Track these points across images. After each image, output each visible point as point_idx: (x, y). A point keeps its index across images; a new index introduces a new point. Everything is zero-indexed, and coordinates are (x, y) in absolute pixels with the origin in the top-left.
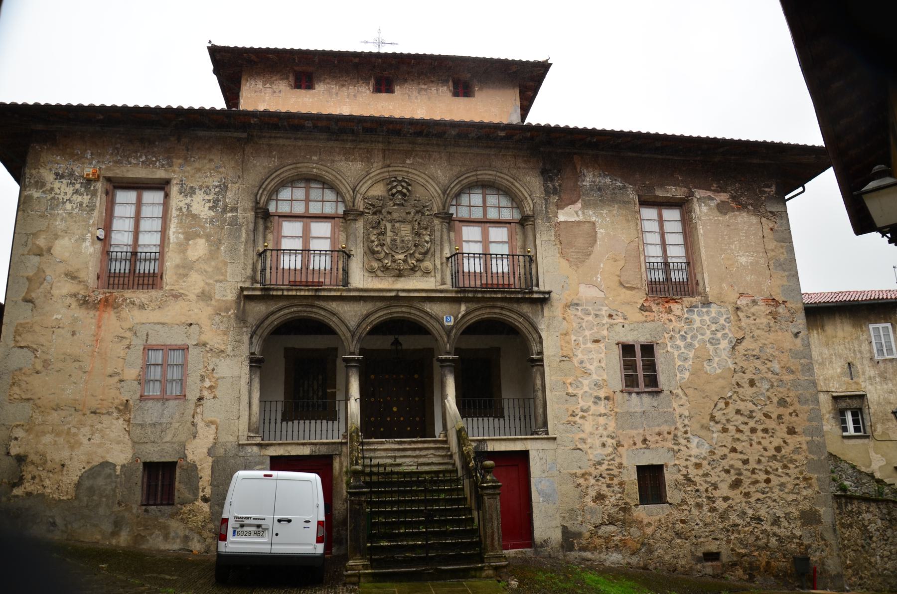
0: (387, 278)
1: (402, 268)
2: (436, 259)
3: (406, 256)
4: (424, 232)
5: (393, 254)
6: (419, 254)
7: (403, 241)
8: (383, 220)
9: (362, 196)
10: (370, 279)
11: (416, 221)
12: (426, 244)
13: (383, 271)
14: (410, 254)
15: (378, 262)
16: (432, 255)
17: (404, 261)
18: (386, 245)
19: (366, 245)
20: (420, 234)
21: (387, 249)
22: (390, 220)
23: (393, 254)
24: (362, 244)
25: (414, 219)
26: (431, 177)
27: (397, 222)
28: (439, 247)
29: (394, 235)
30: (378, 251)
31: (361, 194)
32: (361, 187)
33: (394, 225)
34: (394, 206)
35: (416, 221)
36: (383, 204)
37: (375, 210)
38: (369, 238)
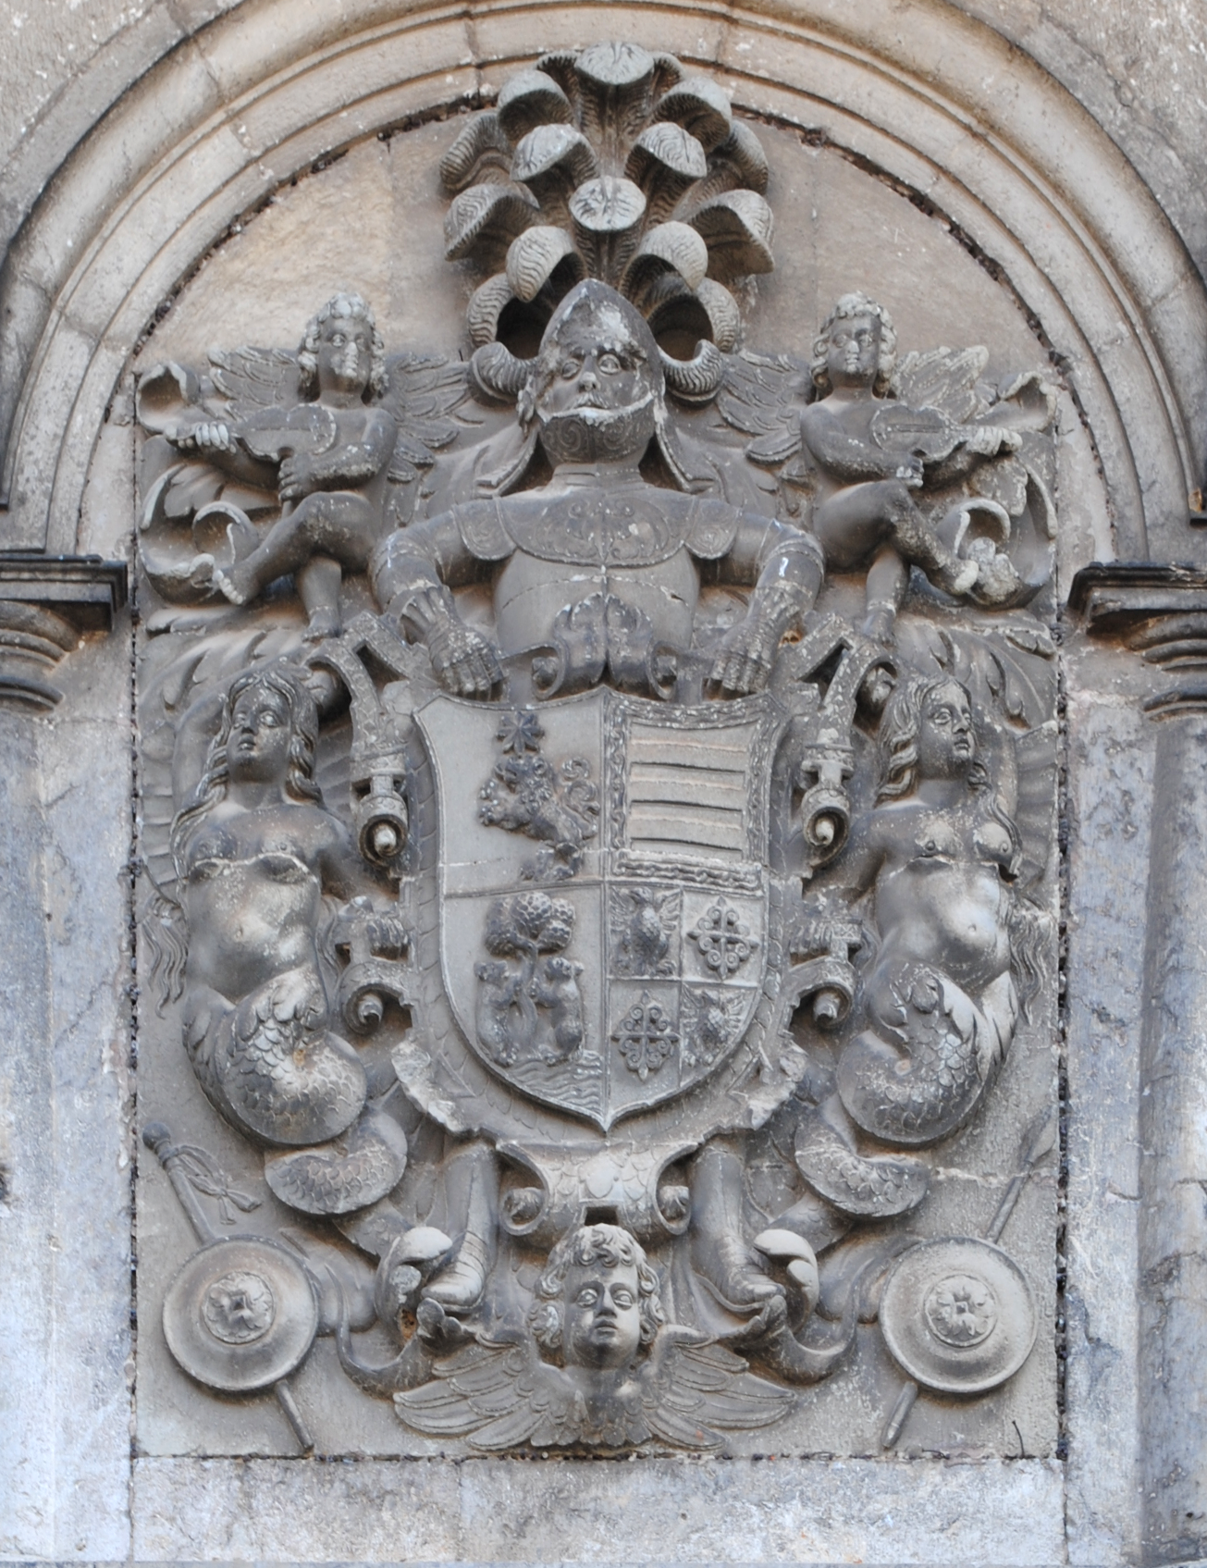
0: (439, 1485)
1: (628, 1323)
2: (1083, 1216)
3: (681, 1167)
4: (939, 830)
5: (519, 1132)
6: (865, 1140)
7: (649, 947)
8: (380, 673)
9: (109, 363)
10: (217, 1492)
11: (823, 674)
12: (955, 998)
13: (377, 1388)
14: (749, 1141)
15: (323, 1259)
16: (1027, 1155)
17: (654, 1241)
18: (429, 1019)
19: (162, 1031)
20: (881, 858)
21: (438, 1076)
22: (483, 658)
23: (519, 1132)
24: (108, 1026)
25: (808, 653)
26: (1041, 42)
27: (574, 684)
28: (1123, 1058)
29: (529, 874)
30: (313, 1105)
31: (98, 338)
32: (96, 228)
33: (532, 737)
34: (537, 470)
35: (823, 674)
36: (386, 451)
37: (276, 533)
38: (195, 926)
